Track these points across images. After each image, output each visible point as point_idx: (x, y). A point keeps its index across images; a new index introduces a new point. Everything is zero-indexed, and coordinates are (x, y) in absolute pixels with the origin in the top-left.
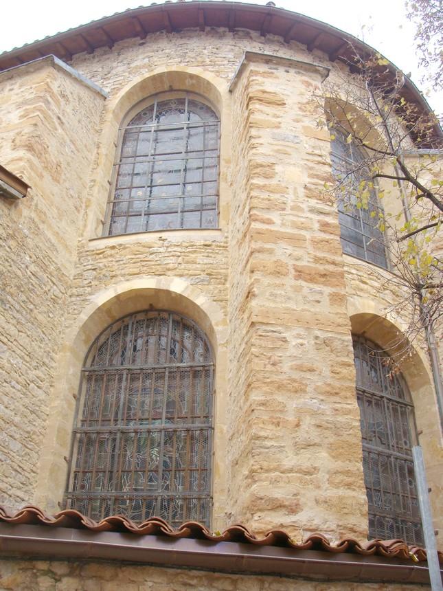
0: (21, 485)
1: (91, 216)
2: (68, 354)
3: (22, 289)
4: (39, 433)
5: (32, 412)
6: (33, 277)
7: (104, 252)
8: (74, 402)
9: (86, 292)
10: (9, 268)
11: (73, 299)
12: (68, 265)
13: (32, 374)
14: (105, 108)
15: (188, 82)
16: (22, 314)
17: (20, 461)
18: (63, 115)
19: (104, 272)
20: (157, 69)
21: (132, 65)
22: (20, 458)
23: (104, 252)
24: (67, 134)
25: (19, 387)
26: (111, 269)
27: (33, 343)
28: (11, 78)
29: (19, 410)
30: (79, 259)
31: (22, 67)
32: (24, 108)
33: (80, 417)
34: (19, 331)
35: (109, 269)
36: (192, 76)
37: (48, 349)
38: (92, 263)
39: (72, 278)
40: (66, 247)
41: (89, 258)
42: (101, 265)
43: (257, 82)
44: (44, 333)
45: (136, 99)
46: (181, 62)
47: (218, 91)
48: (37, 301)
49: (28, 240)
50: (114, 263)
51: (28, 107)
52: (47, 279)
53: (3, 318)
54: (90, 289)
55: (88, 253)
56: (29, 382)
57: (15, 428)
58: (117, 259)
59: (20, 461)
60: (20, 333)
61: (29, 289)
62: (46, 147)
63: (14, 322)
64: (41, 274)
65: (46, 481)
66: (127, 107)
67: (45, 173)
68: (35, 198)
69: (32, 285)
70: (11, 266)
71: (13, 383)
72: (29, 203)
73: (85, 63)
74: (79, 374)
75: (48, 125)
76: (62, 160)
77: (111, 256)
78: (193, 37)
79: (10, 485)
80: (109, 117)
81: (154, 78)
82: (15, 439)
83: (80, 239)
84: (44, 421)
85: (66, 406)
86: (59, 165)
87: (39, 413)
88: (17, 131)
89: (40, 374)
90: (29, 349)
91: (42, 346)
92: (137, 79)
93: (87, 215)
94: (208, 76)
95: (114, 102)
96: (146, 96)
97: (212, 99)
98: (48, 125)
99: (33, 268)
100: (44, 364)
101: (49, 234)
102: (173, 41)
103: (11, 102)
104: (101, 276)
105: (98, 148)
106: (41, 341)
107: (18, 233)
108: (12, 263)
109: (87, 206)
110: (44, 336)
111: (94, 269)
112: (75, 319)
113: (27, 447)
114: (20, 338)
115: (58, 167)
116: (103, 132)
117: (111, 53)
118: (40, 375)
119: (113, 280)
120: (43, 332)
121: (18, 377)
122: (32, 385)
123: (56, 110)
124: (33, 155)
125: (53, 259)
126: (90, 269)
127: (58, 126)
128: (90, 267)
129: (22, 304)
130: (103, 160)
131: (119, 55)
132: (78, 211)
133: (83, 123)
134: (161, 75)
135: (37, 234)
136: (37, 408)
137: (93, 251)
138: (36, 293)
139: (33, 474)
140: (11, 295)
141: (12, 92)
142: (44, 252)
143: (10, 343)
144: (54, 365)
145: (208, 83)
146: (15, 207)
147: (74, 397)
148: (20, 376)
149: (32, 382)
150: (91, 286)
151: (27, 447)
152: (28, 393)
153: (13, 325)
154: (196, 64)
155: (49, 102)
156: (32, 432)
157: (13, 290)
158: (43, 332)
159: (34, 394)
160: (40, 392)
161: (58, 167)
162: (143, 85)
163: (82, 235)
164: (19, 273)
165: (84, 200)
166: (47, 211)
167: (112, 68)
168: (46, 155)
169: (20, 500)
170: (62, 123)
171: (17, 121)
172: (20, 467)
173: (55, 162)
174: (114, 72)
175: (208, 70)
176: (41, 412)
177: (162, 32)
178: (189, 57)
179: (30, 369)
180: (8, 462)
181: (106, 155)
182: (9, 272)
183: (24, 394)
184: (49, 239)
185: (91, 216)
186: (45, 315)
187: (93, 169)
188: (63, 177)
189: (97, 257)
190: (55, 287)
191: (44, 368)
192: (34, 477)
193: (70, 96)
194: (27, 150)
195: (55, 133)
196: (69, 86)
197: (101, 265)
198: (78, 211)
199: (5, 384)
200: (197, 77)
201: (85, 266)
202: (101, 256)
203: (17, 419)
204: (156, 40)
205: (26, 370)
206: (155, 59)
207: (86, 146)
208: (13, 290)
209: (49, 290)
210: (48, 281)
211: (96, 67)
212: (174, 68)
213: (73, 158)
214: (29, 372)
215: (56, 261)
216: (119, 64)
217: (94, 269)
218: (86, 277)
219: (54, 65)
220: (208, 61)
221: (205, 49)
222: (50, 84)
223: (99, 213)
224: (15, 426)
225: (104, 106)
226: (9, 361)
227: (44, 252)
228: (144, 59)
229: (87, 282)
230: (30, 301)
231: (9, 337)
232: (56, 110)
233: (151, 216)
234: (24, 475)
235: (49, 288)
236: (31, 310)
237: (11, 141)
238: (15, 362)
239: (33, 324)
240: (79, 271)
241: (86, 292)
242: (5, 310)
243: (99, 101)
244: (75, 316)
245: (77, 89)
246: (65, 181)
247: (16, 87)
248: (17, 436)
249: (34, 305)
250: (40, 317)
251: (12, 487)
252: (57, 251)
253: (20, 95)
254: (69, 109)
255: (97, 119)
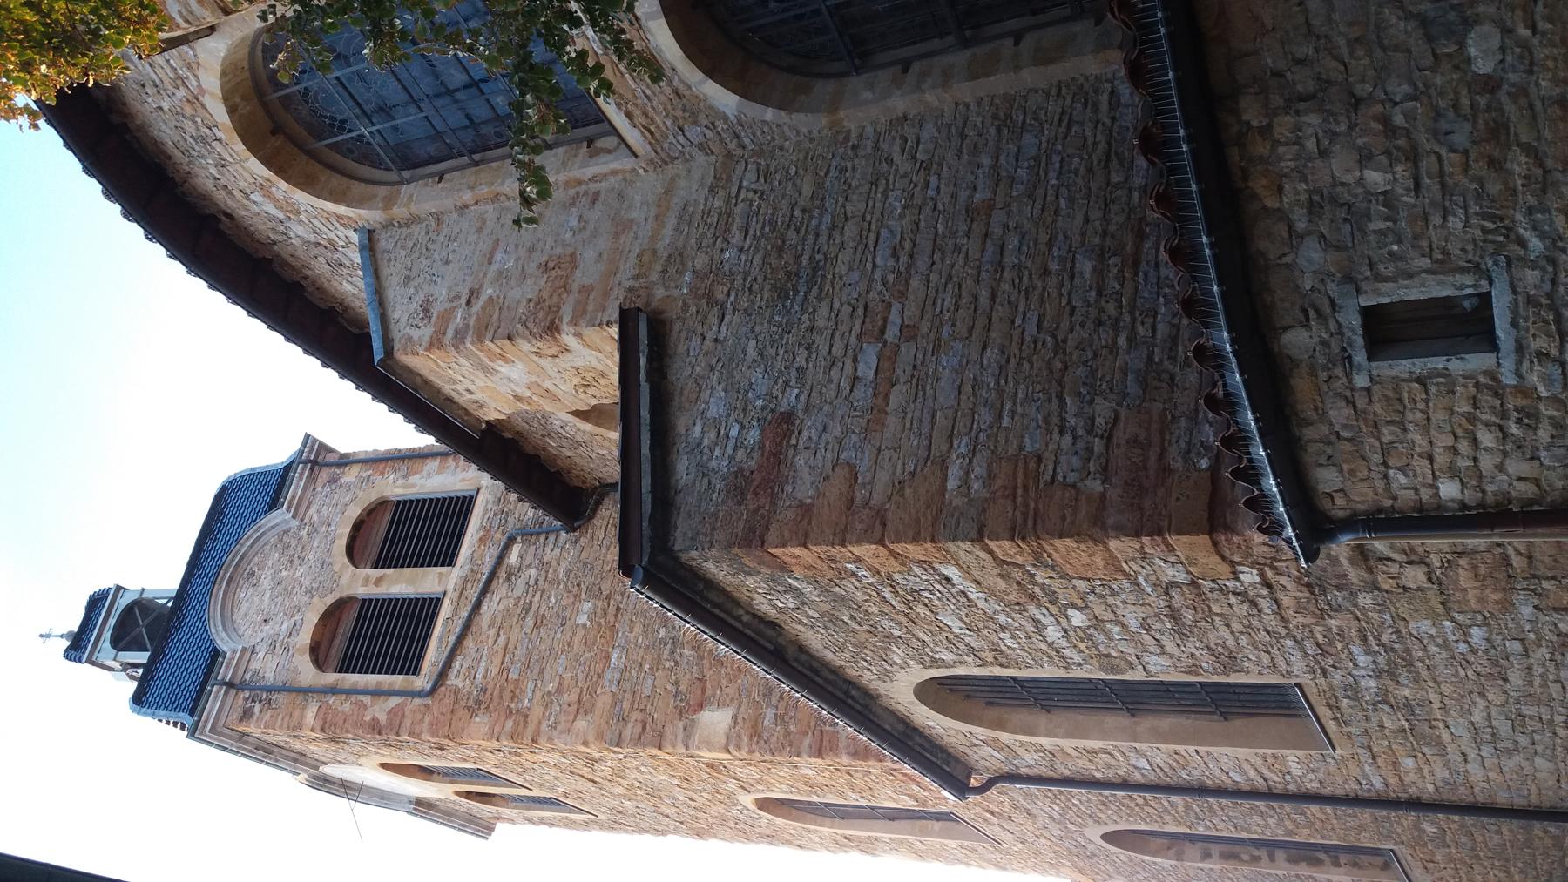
0: (1089, 107)
1: (590, 171)
2: (842, 114)
3: (780, 242)
4: (993, 108)
5: (963, 136)
6: (751, 232)
7: (643, 126)
8: (916, 67)
9: (725, 127)
10: (760, 280)
11: (747, 141)
12: (697, 174)
13: (904, 166)
14: (389, 224)
15: (245, 109)
16: (819, 225)
17: (1051, 125)
18: (457, 297)
19: (679, 113)
20: (260, 173)
21: (281, 215)
22: (1046, 126)
23: (643, 126)
24: (485, 274)
25: (933, 180)
26: (668, 103)
27: (853, 185)
28: (450, 400)
29: (969, 163)
30: (677, 158)
31: (422, 395)
32: (490, 363)
33: (935, 44)
34: (847, 219)
35: (669, 107)
36: (232, 110)
37: (850, 152)
38: (671, 137)
39: (713, 158)
40: (668, 192)
41: (666, 146)
42: (669, 123)
43: (183, 11)
44: (828, 171)
45: (337, 181)
46: (219, 140)
47: (228, 50)
48: (784, 206)
49: (698, 266)
50: (655, 104)
51: (486, 360)
52: (741, 205)
53: (840, 256)
54: (717, 123)
55: (659, 150)
56: (918, 165)
57: (1001, 158)
58: (646, 100)
59: (1051, 125)
60: (849, 215)
61: (773, 231)
62: (532, 304)
63: (836, 233)
64: (738, 220)
65: (1067, 64)
66: (358, 188)
67: (575, 287)
68: (627, 284)
69: (763, 228)
70: (756, 279)
71: (931, 193)
72: (642, 293)
73: (326, 285)
74: (865, 76)
75: (495, 316)
76: (533, 265)
77: (645, 114)
78: (153, 138)
79: (1096, 127)
80: (399, 211)
81: (280, 171)
82: (1019, 150)
83: (641, 171)
84: (967, 106)
85: (929, 81)
86: (545, 268)
87: (960, 122)
88: (536, 359)
89: (897, 148)
90: (866, 188)
91: (849, 165)
92: (301, 197)
93: (594, 177)
94: (210, 81)
95: (369, 216)
96: (320, 167)
97: (247, 50)
98: (495, 316)
99: (736, 236)
100: (876, 148)
101: (668, 232)
102: (187, 168)
103: (489, 384)
104: (687, 115)
105: (466, 206)
106: (843, 170)
107: (698, 289)
108: (750, 279)
109: (580, 183)
110: (832, 169)
111: (682, 130)
112: (778, 126)
113: (1024, 120)
114: (857, 213)
115: (551, 265)
116: (434, 210)
117: (278, 256)
118: (898, 149)
119: (687, 93)
120: (826, 175)
121: (919, 188)
122: (920, 156)
123: (459, 314)
124: (561, 319)
125: (702, 207)
126: (684, 135)
127: (484, 298)
128: (681, 138)
129: (803, 233)
130: (484, 190)
131: (275, 243)
132: (597, 194)
133: (445, 254)
134: (267, 162)
135: (681, 255)
136: (953, 130)
137: (651, 144)
138: (773, 214)
139: (1064, 91)
140: (798, 258)
141: (471, 387)
142: (700, 230)
143: (873, 227)
144: (869, 130)
145: (224, 74)
146: (661, 313)
147: (905, 70)
148: (916, 186)
149: (914, 157)
150: (713, 124)
151: (1024, 120)
152: (936, 158)
153: (842, 234)
154: (201, 111)
155: (457, 332)
156: (996, 123)
157: (788, 257)
158: (826, 175)
159: (932, 146)
160: (925, 136)
161: (551, 265)
162: (306, 183)
163: (633, 170)
164: (757, 260)
165: (572, 192)
166: (633, 255)
167: (307, 243)
168: (545, 295)
169: (1115, 99)
170: (472, 293)
171: (520, 366)
172: (1060, 120)
173: (545, 276)
174: (312, 238)
175: (200, 86)
176: (956, 118)
177: (183, 192)
178: (198, 130)
179: (897, 170)
180: (1060, 147)
181: (472, 188)
182: (765, 277)
183: (940, 165)
184: (676, 230)
185: (590, 171)
186: (798, 182)
187: (508, 199)
188: (559, 250)
189: (657, 135)
190: (745, 184)
191: (885, 146)
192: (1068, 87)
193: (420, 297)
194: (559, 333)
195: (498, 297)
196: (402, 310)
197: (669, 123)
198: (597, 194)
199: (940, 207)
200: (227, 99)
201: (683, 147)
202: (652, 128)
203: (986, 161)
204: (206, 197)
205: (901, 177)
206: (242, 184)
207: (479, 230)
208: (788, 257)
209: (756, 192)
210: (743, 201)
211: (320, 267)
212: (239, 146)
213: (516, 246)
214: (902, 172)
215: (702, 201)
216: (292, 235)
217: (682, 130)
218: (701, 137)
219: (389, 351)
220: (181, 93)
221: (161, 108)
222: (425, 344)
223: (579, 158)
224: (997, 160)
225: (385, 227)
226: (902, 216)
227: (700, 230)
228: (255, 202)
229: (707, 132)
230: (790, 220)
231: (864, 233)
232: (459, 314)
233: (859, 374)
234: (1071, 106)
235: (751, 195)
236: (804, 211)
237: (557, 360)
238: (898, 204)
239: (823, 199)
240: (696, 152)
241: (725, 127)
242: (826, 259)
243: (385, 242)
244: (774, 127)
245: (394, 293)
246: (564, 245)
247: (460, 388)
248: (1013, 148)
249: (793, 210)
250: (807, 190)
251: (1098, 122)
252: (686, 205)
253: (472, 377)
254: (441, 292)
255: (417, 229)
